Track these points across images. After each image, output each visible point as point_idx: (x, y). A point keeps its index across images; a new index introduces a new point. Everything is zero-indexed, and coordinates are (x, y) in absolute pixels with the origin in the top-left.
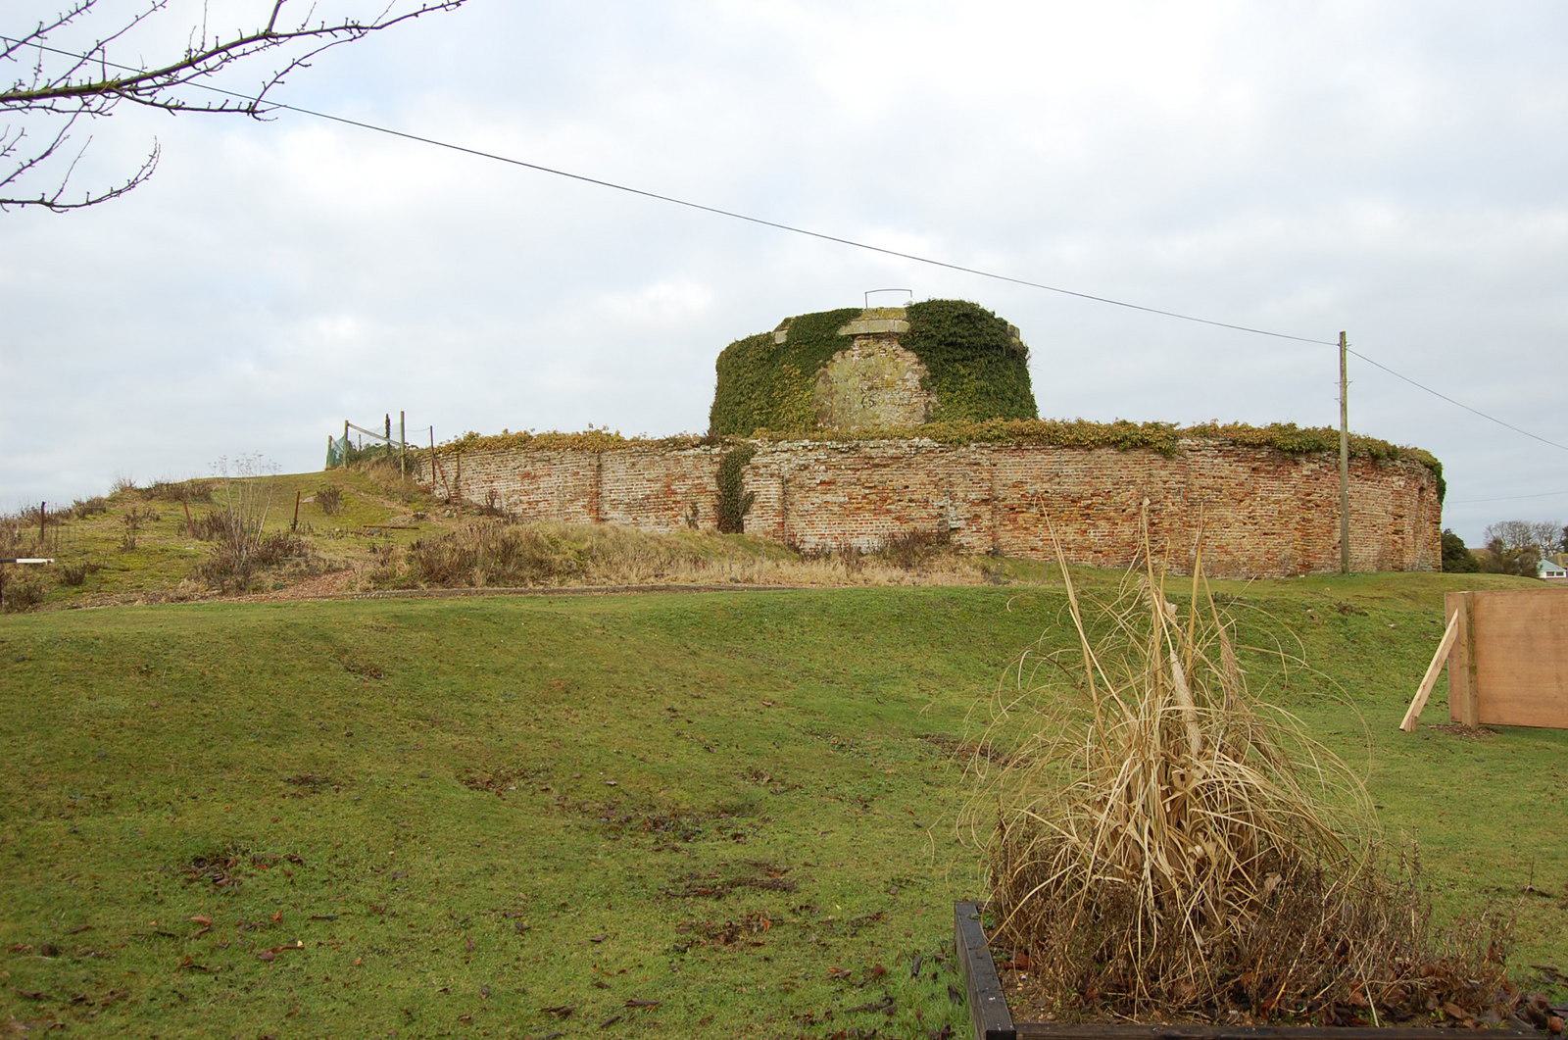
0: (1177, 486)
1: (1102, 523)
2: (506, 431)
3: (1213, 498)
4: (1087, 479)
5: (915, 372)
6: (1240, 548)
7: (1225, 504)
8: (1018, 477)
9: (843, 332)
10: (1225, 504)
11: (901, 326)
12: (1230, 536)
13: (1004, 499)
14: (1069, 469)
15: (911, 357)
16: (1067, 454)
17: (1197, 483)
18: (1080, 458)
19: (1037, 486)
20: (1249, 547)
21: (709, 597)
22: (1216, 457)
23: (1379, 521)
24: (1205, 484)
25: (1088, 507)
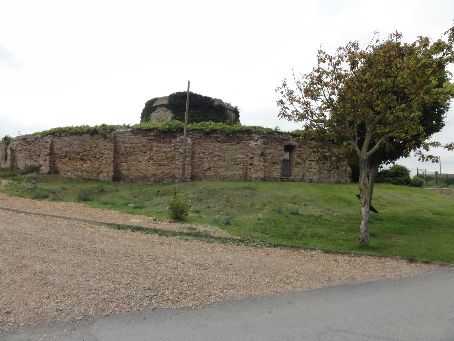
0: (109, 147)
1: (89, 162)
2: (410, 172)
3: (131, 151)
4: (81, 146)
5: (170, 116)
6: (147, 171)
7: (137, 154)
8: (60, 146)
9: (154, 105)
10: (137, 154)
11: (166, 102)
12: (143, 165)
13: (58, 154)
14: (75, 143)
15: (170, 112)
16: (74, 137)
17: (123, 146)
18: (78, 139)
19: (66, 149)
20: (152, 170)
21: (136, 220)
22: (131, 135)
23: (239, 160)
24: (126, 146)
25: (83, 156)
